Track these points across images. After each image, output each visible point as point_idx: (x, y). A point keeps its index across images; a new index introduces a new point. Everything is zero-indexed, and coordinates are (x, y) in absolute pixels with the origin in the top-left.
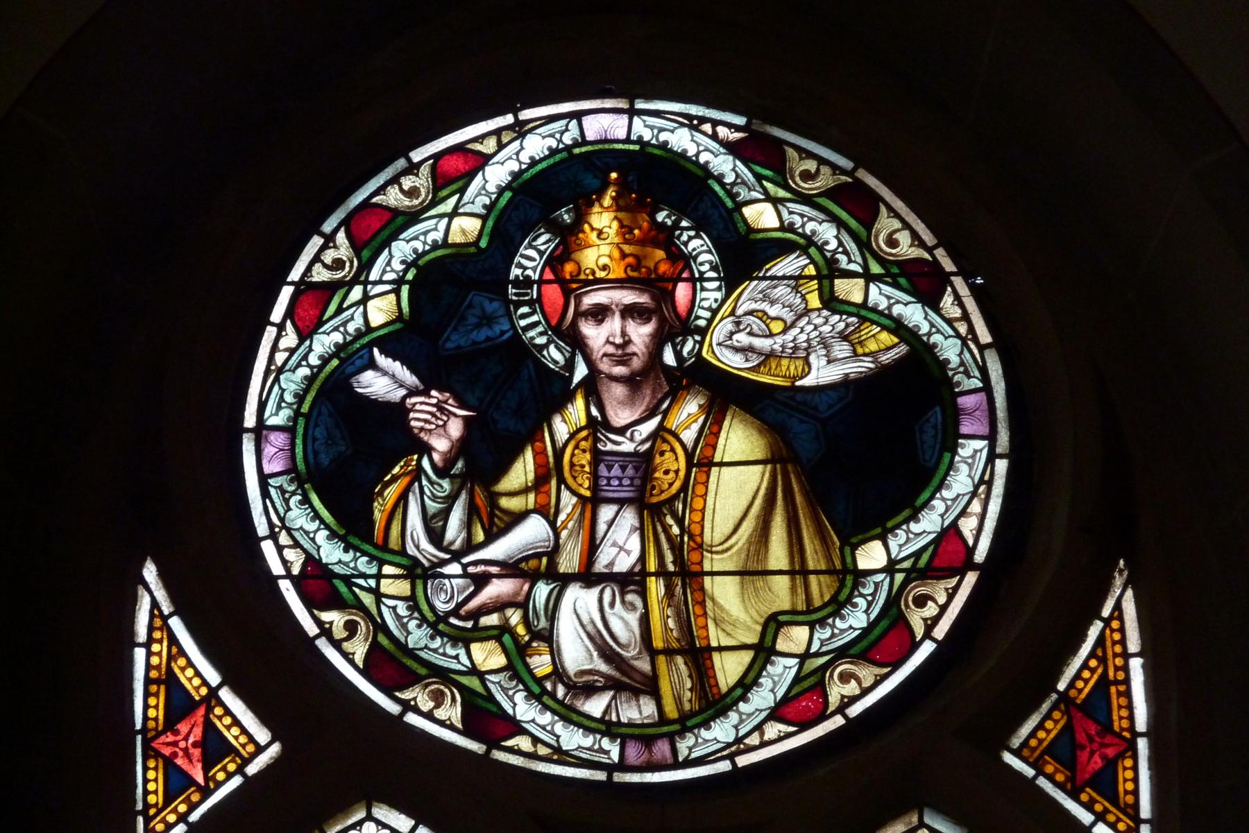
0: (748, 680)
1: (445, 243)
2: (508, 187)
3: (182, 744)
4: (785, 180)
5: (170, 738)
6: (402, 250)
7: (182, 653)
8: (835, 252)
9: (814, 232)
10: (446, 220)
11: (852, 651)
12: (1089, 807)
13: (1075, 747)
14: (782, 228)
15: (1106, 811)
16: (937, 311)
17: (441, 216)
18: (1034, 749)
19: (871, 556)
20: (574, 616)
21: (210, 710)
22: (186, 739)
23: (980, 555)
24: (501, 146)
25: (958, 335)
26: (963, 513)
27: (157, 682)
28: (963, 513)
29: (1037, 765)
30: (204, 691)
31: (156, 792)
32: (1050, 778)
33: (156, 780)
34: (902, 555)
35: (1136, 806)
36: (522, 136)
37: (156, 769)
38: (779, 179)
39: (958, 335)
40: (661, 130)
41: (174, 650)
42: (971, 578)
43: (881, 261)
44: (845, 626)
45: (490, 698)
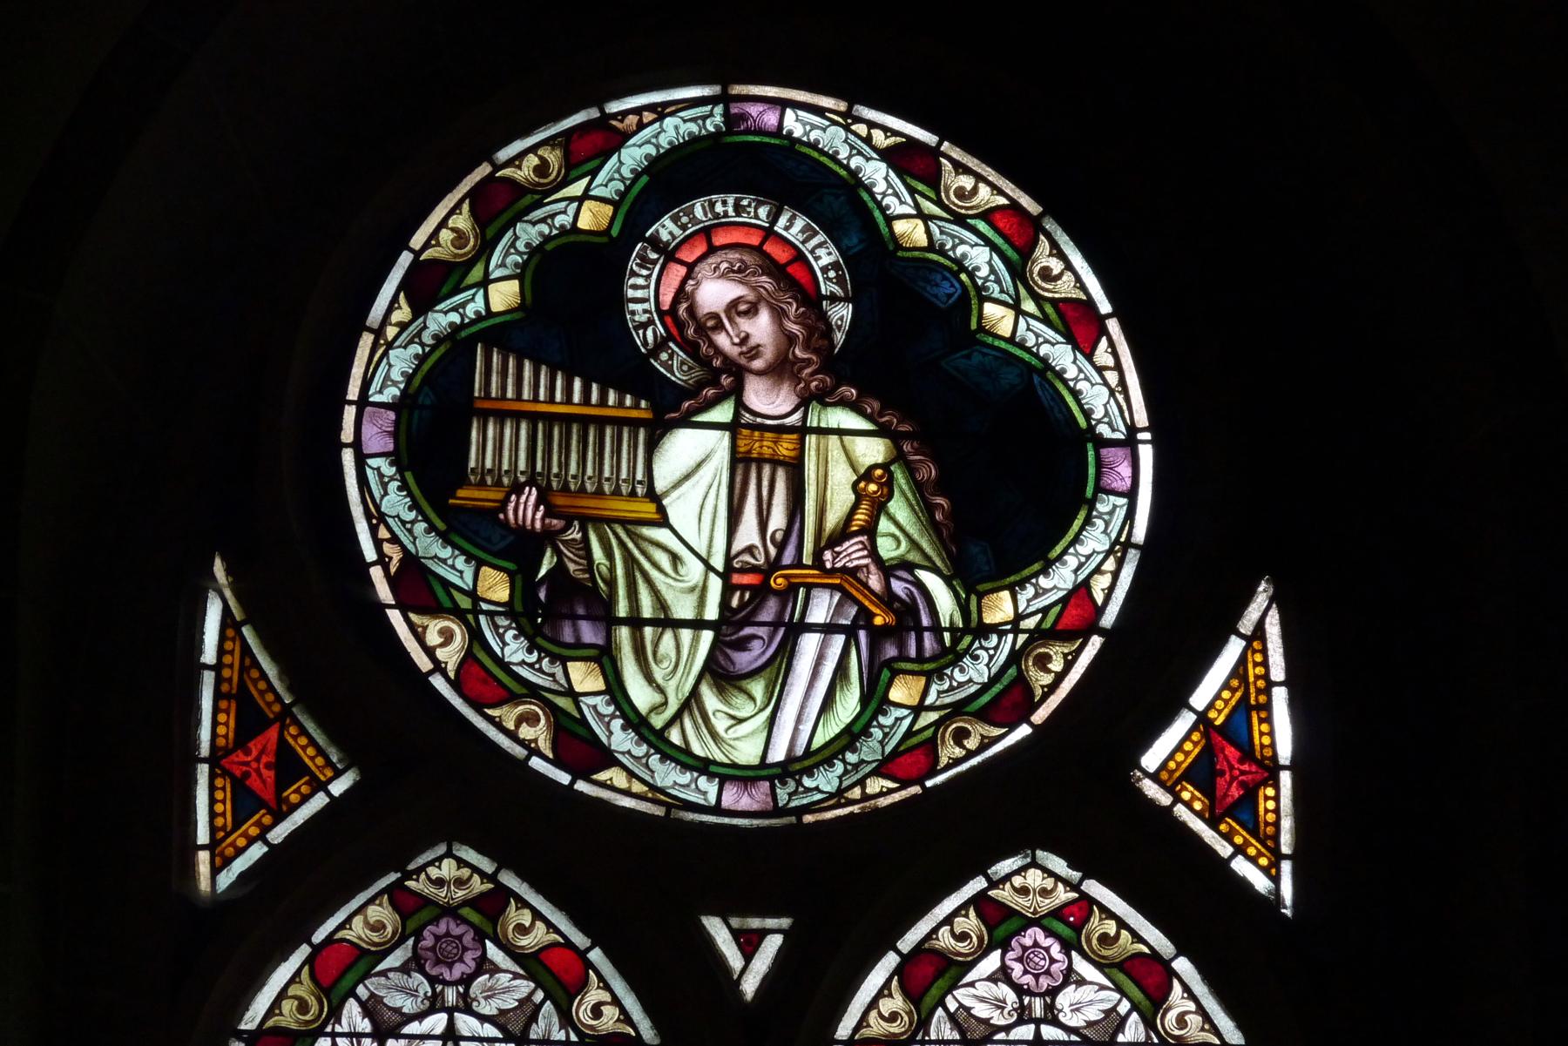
2: (646, 171)
3: (254, 765)
4: (938, 194)
6: (528, 233)
8: (986, 279)
9: (964, 256)
10: (575, 205)
11: (970, 709)
12: (1228, 837)
13: (1215, 774)
14: (931, 247)
15: (1247, 843)
16: (1089, 357)
17: (571, 199)
18: (1172, 772)
19: (1000, 608)
21: (283, 728)
23: (1108, 619)
25: (1106, 383)
26: (1098, 570)
29: (1170, 790)
30: (277, 708)
31: (223, 814)
32: (1188, 805)
33: (224, 789)
34: (1031, 609)
35: (1276, 837)
37: (224, 789)
39: (1106, 383)
40: (814, 127)
41: (247, 661)
42: (1096, 642)
45: (583, 721)
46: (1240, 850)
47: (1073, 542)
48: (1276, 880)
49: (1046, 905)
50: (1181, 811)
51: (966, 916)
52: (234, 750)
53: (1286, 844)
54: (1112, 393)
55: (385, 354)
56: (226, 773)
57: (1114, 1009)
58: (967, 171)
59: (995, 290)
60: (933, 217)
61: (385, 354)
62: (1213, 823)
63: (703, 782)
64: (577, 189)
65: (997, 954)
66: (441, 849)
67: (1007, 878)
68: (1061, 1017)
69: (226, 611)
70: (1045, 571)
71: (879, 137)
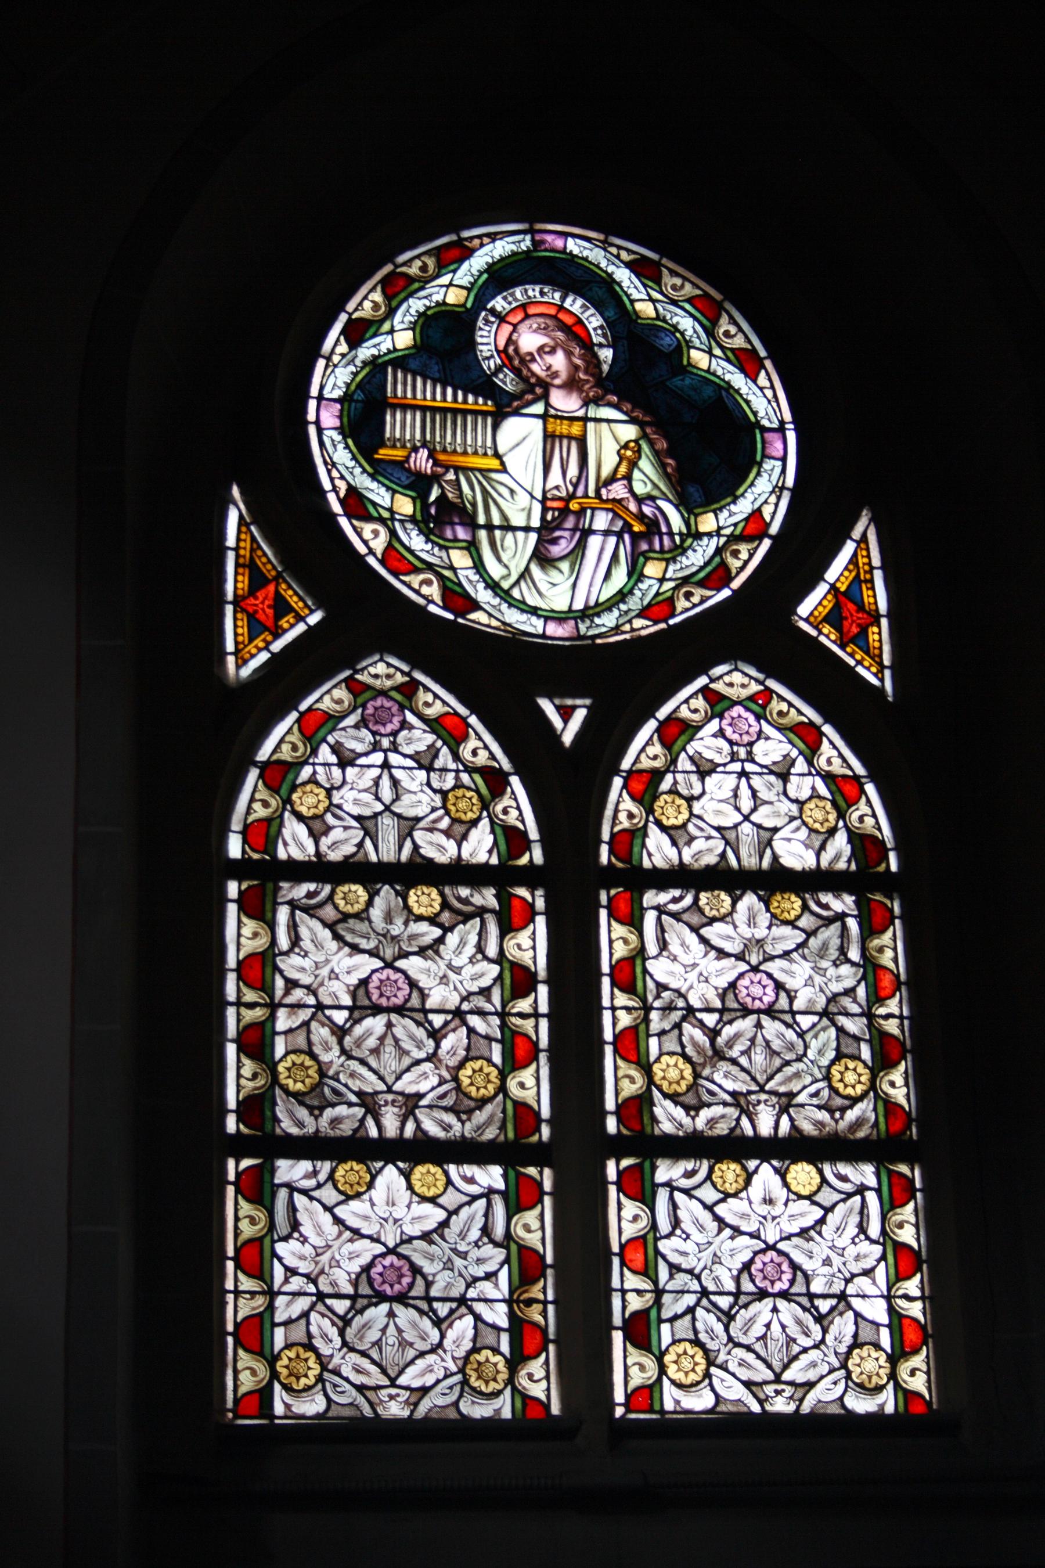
0: (625, 590)
1: (444, 303)
2: (486, 271)
4: (517, 1289)
5: (252, 601)
6: (416, 305)
7: (260, 547)
14: (658, 318)
15: (863, 659)
16: (755, 381)
19: (707, 523)
20: (521, 438)
22: (263, 603)
23: (774, 529)
24: (482, 245)
27: (244, 566)
28: (766, 502)
35: (880, 656)
36: (493, 241)
38: (657, 288)
42: (767, 543)
43: (722, 348)
44: (688, 563)
48: (882, 680)
67: (721, 677)
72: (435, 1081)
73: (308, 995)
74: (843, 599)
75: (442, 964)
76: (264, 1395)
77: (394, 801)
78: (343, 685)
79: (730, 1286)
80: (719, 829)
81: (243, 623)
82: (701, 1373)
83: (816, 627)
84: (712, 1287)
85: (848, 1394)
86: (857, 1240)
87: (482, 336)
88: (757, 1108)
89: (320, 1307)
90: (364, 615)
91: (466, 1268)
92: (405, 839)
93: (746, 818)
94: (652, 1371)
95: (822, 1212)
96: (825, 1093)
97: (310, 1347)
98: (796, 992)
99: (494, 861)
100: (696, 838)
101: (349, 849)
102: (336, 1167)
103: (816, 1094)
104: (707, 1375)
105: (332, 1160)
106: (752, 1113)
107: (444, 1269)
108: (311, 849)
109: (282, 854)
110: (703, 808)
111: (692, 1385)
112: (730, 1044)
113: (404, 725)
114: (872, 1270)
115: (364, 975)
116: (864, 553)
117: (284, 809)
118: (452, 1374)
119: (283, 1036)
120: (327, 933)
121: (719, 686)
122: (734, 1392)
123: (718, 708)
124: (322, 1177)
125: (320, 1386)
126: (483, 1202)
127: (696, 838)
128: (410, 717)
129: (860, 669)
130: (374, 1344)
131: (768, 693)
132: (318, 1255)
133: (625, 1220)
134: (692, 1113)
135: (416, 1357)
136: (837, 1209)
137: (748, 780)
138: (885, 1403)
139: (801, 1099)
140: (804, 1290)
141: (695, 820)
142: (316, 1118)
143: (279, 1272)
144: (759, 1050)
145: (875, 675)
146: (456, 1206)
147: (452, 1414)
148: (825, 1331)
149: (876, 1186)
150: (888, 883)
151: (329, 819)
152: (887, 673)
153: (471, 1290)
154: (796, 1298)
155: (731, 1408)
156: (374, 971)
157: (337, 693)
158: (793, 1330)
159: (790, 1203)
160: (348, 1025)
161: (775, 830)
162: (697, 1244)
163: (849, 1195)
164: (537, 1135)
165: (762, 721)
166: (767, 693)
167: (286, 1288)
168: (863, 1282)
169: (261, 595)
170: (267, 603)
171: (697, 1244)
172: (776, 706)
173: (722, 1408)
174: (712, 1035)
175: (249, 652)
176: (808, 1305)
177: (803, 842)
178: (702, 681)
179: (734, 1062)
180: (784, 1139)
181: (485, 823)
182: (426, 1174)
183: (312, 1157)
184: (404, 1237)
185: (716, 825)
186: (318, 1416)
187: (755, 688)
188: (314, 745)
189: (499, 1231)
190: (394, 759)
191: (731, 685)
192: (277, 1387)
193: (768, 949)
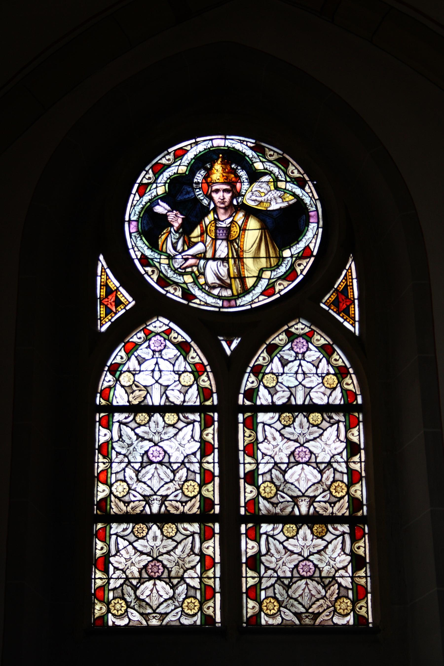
2: (194, 158)
5: (106, 300)
6: (167, 174)
12: (342, 317)
13: (339, 302)
14: (264, 169)
15: (347, 318)
16: (304, 190)
18: (328, 303)
19: (286, 253)
21: (117, 293)
22: (111, 300)
23: (315, 253)
27: (103, 285)
30: (115, 288)
32: (333, 310)
35: (355, 317)
41: (108, 277)
46: (345, 320)
47: (304, 236)
48: (354, 327)
49: (302, 332)
50: (331, 311)
51: (283, 335)
52: (105, 298)
53: (357, 318)
54: (311, 198)
55: (134, 208)
56: (103, 304)
57: (319, 357)
58: (272, 150)
59: (280, 178)
60: (264, 162)
61: (134, 208)
62: (339, 314)
63: (218, 301)
64: (178, 163)
65: (290, 344)
66: (156, 319)
67: (293, 326)
68: (306, 359)
69: (102, 266)
70: (298, 243)
71: (249, 144)
72: (322, 490)
73: (124, 458)
74: (340, 294)
75: (177, 443)
76: (257, 616)
77: (160, 378)
78: (284, 333)
79: (137, 575)
80: (288, 387)
81: (351, 312)
82: (276, 610)
83: (328, 307)
84: (130, 576)
85: (334, 617)
86: (121, 556)
87: (197, 192)
88: (153, 502)
89: (279, 582)
90: (150, 304)
91: (335, 564)
92: (163, 395)
93: (157, 382)
94: (104, 610)
95: (176, 544)
96: (180, 495)
97: (123, 598)
98: (318, 454)
99: (342, 403)
100: (279, 391)
101: (285, 400)
102: (135, 526)
103: (176, 496)
104: (279, 610)
105: (133, 523)
106: (150, 504)
107: (326, 565)
108: (270, 400)
109: (258, 403)
110: (282, 379)
111: (272, 615)
112: (144, 476)
113: (308, 349)
114: (346, 566)
115: (146, 449)
116: (350, 274)
117: (116, 383)
118: (330, 607)
119: (115, 474)
120: (278, 434)
121: (293, 330)
122: (289, 617)
123: (292, 338)
124: (129, 530)
125: (279, 613)
126: (341, 538)
127: (279, 391)
128: (311, 346)
129: (113, 320)
130: (300, 596)
131: (171, 329)
132: (277, 561)
133: (248, 547)
134: (126, 505)
135: (164, 601)
136: (333, 542)
137: (303, 369)
138: (349, 620)
139: (171, 498)
140: (318, 576)
141: (279, 384)
142: (127, 507)
143: (111, 569)
144: (155, 478)
145: (352, 325)
146: (331, 539)
147: (330, 623)
148: (326, 592)
149: (199, 532)
150: (358, 409)
151: (277, 388)
152: (357, 324)
153: (337, 573)
154: (164, 579)
155: (288, 623)
156: (296, 448)
157: (139, 335)
158: (314, 592)
159: (314, 540)
160: (140, 469)
161: (312, 388)
162: (125, 559)
163: (338, 536)
164: (361, 511)
165: (309, 344)
166: (170, 330)
167: (114, 576)
168: (342, 572)
169: (110, 297)
170: (112, 300)
171: (125, 559)
172: (173, 335)
173: (131, 624)
174: (137, 473)
175: (105, 321)
176: (320, 581)
177: (179, 391)
178: (286, 327)
179: (145, 483)
180: (162, 514)
181: (195, 387)
182: (170, 529)
183: (128, 522)
184: (311, 553)
185: (287, 386)
186: (278, 625)
187: (165, 328)
188: (272, 357)
189: (197, 550)
190: (303, 362)
191: (297, 329)
192: (263, 614)
193: (162, 436)
